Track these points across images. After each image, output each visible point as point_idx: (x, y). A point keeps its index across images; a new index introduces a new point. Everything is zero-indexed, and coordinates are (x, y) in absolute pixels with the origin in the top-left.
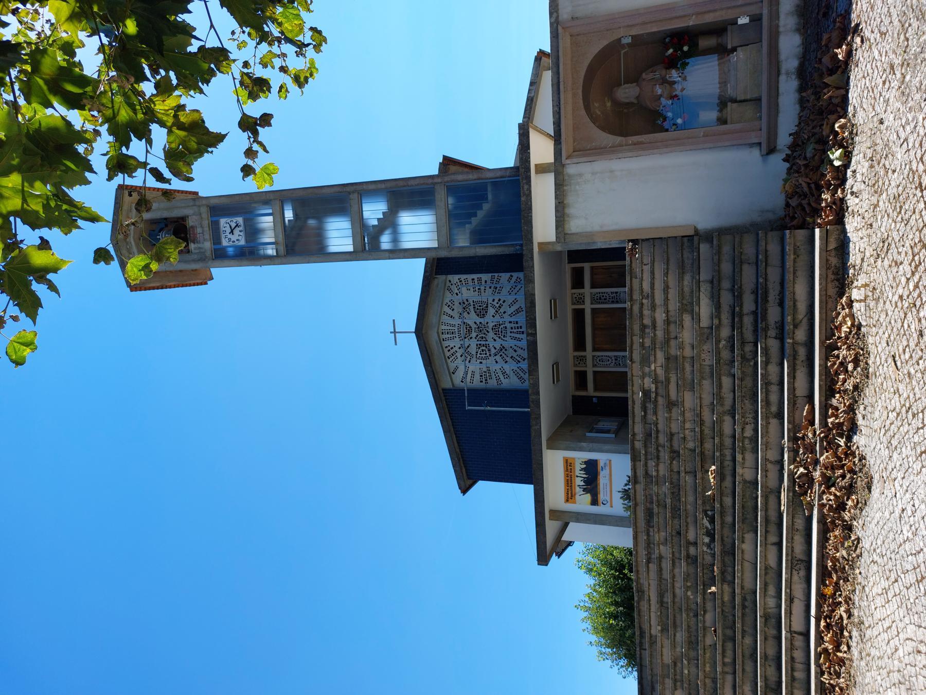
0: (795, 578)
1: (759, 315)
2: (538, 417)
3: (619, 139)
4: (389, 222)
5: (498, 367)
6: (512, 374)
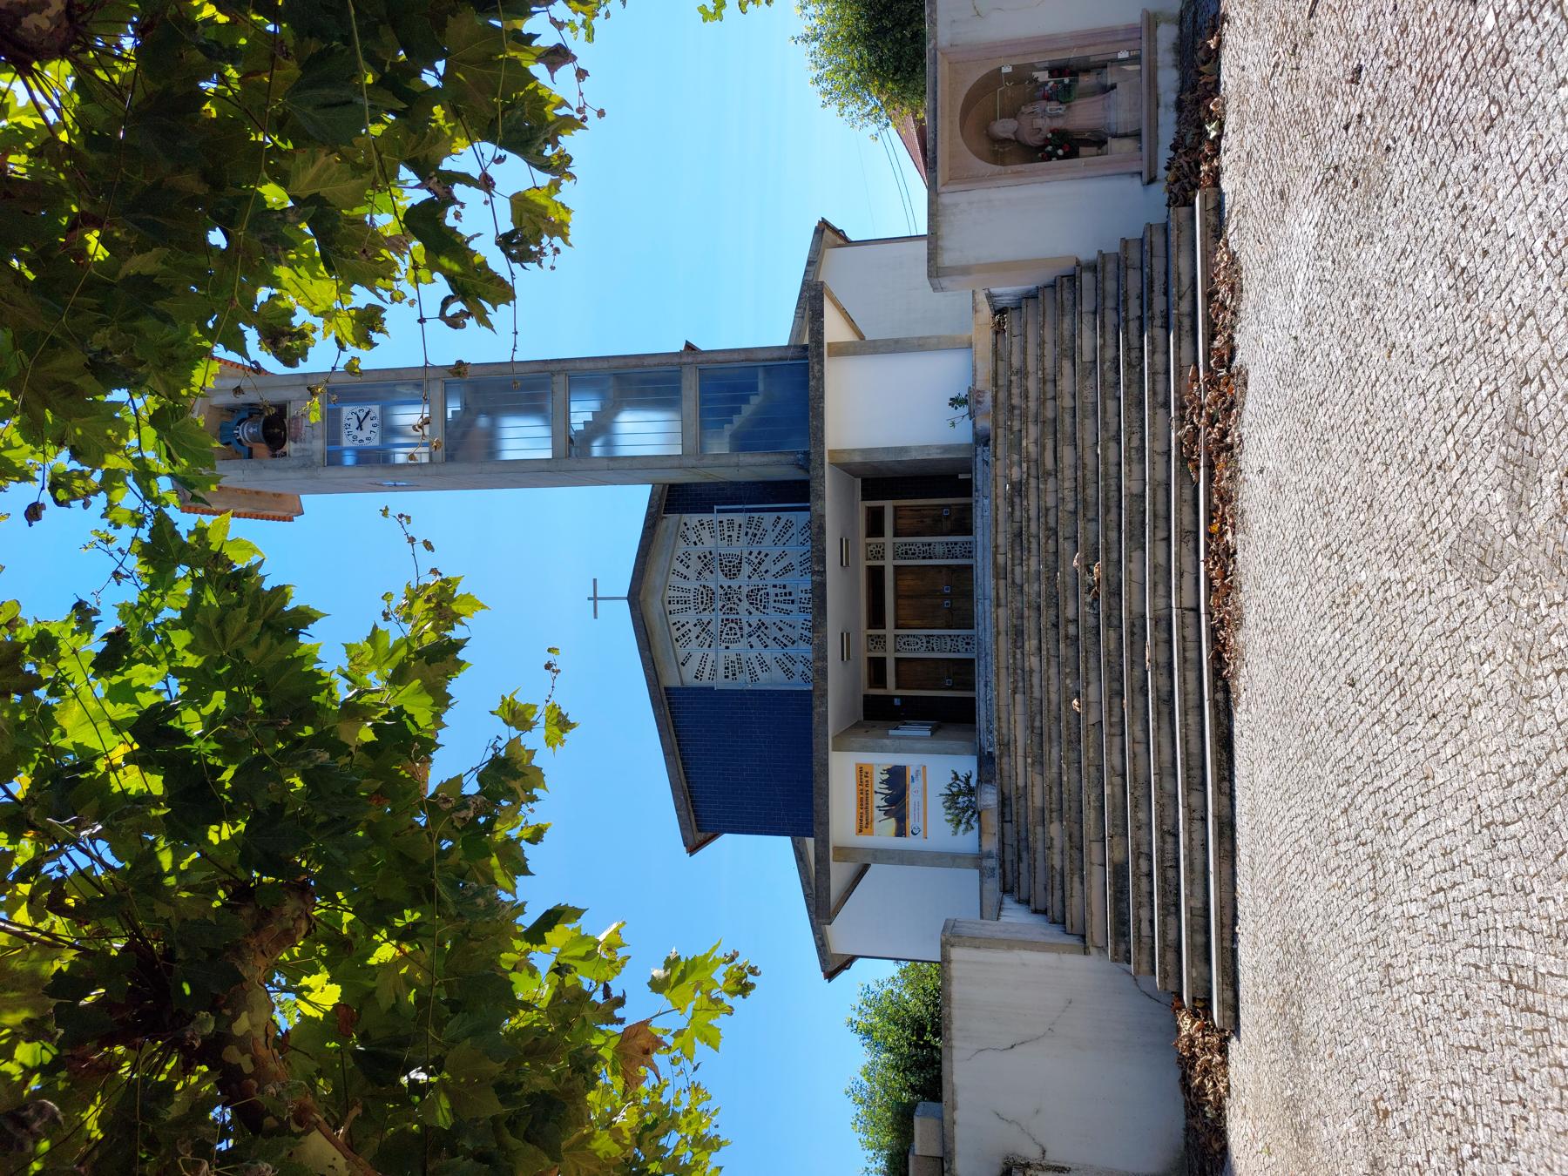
0: (1185, 550)
1: (1146, 301)
2: (824, 695)
3: (998, 168)
4: (602, 426)
5: (753, 654)
6: (774, 666)
